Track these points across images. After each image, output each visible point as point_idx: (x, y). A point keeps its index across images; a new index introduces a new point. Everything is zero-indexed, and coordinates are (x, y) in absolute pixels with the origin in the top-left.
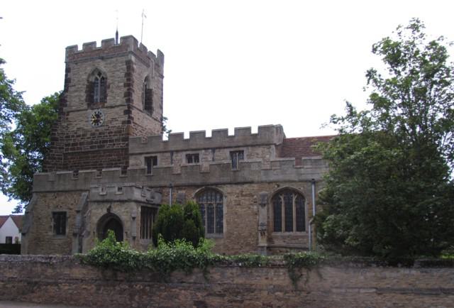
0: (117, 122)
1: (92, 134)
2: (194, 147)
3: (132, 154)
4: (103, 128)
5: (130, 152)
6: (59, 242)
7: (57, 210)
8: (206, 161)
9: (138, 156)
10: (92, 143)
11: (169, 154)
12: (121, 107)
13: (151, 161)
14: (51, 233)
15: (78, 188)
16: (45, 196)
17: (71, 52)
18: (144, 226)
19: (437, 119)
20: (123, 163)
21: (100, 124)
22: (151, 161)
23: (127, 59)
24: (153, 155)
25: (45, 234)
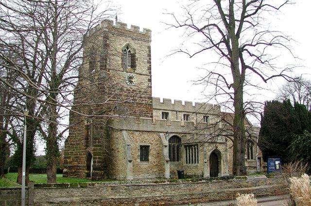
0: (144, 86)
1: (127, 90)
2: (188, 111)
3: (154, 109)
4: (136, 87)
5: (154, 107)
6: (145, 166)
7: (143, 144)
8: (193, 119)
9: (158, 111)
10: (128, 96)
11: (175, 113)
12: (146, 76)
13: (165, 115)
14: (139, 160)
15: (156, 130)
16: (133, 134)
17: (145, 37)
18: (178, 153)
19: (50, 80)
20: (149, 114)
21: (133, 84)
22: (165, 115)
23: (148, 45)
24: (167, 111)
25: (134, 161)
